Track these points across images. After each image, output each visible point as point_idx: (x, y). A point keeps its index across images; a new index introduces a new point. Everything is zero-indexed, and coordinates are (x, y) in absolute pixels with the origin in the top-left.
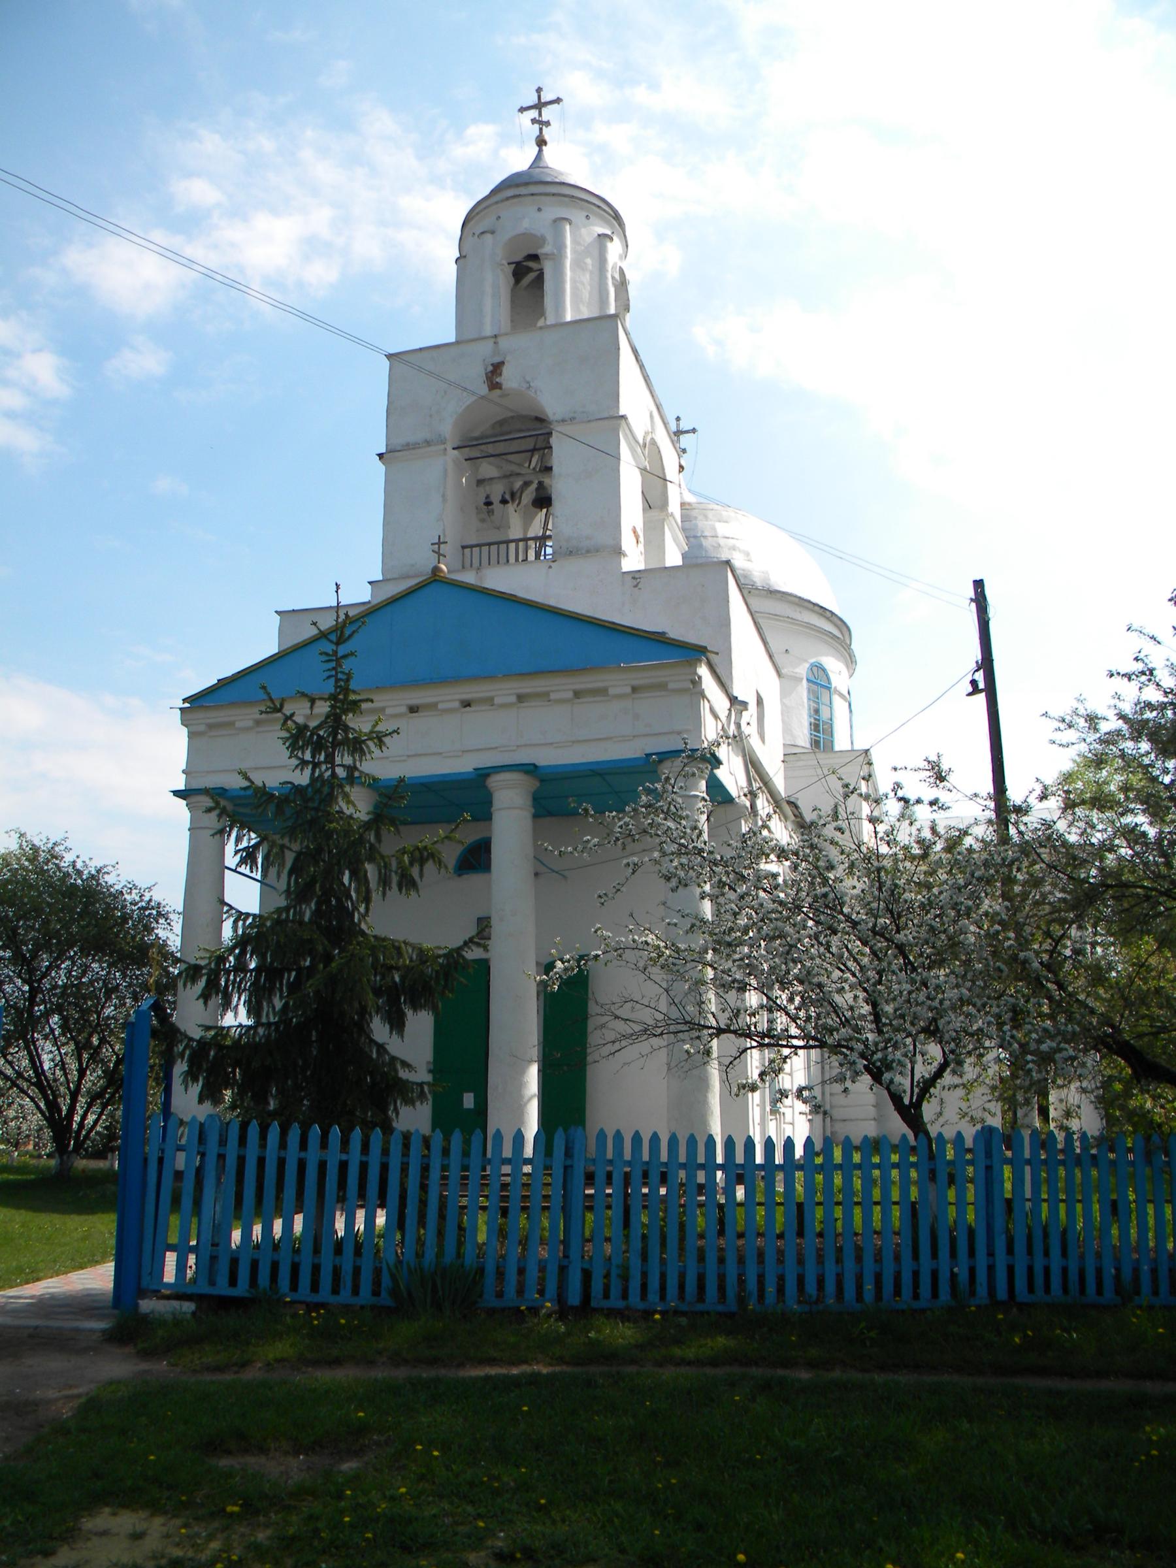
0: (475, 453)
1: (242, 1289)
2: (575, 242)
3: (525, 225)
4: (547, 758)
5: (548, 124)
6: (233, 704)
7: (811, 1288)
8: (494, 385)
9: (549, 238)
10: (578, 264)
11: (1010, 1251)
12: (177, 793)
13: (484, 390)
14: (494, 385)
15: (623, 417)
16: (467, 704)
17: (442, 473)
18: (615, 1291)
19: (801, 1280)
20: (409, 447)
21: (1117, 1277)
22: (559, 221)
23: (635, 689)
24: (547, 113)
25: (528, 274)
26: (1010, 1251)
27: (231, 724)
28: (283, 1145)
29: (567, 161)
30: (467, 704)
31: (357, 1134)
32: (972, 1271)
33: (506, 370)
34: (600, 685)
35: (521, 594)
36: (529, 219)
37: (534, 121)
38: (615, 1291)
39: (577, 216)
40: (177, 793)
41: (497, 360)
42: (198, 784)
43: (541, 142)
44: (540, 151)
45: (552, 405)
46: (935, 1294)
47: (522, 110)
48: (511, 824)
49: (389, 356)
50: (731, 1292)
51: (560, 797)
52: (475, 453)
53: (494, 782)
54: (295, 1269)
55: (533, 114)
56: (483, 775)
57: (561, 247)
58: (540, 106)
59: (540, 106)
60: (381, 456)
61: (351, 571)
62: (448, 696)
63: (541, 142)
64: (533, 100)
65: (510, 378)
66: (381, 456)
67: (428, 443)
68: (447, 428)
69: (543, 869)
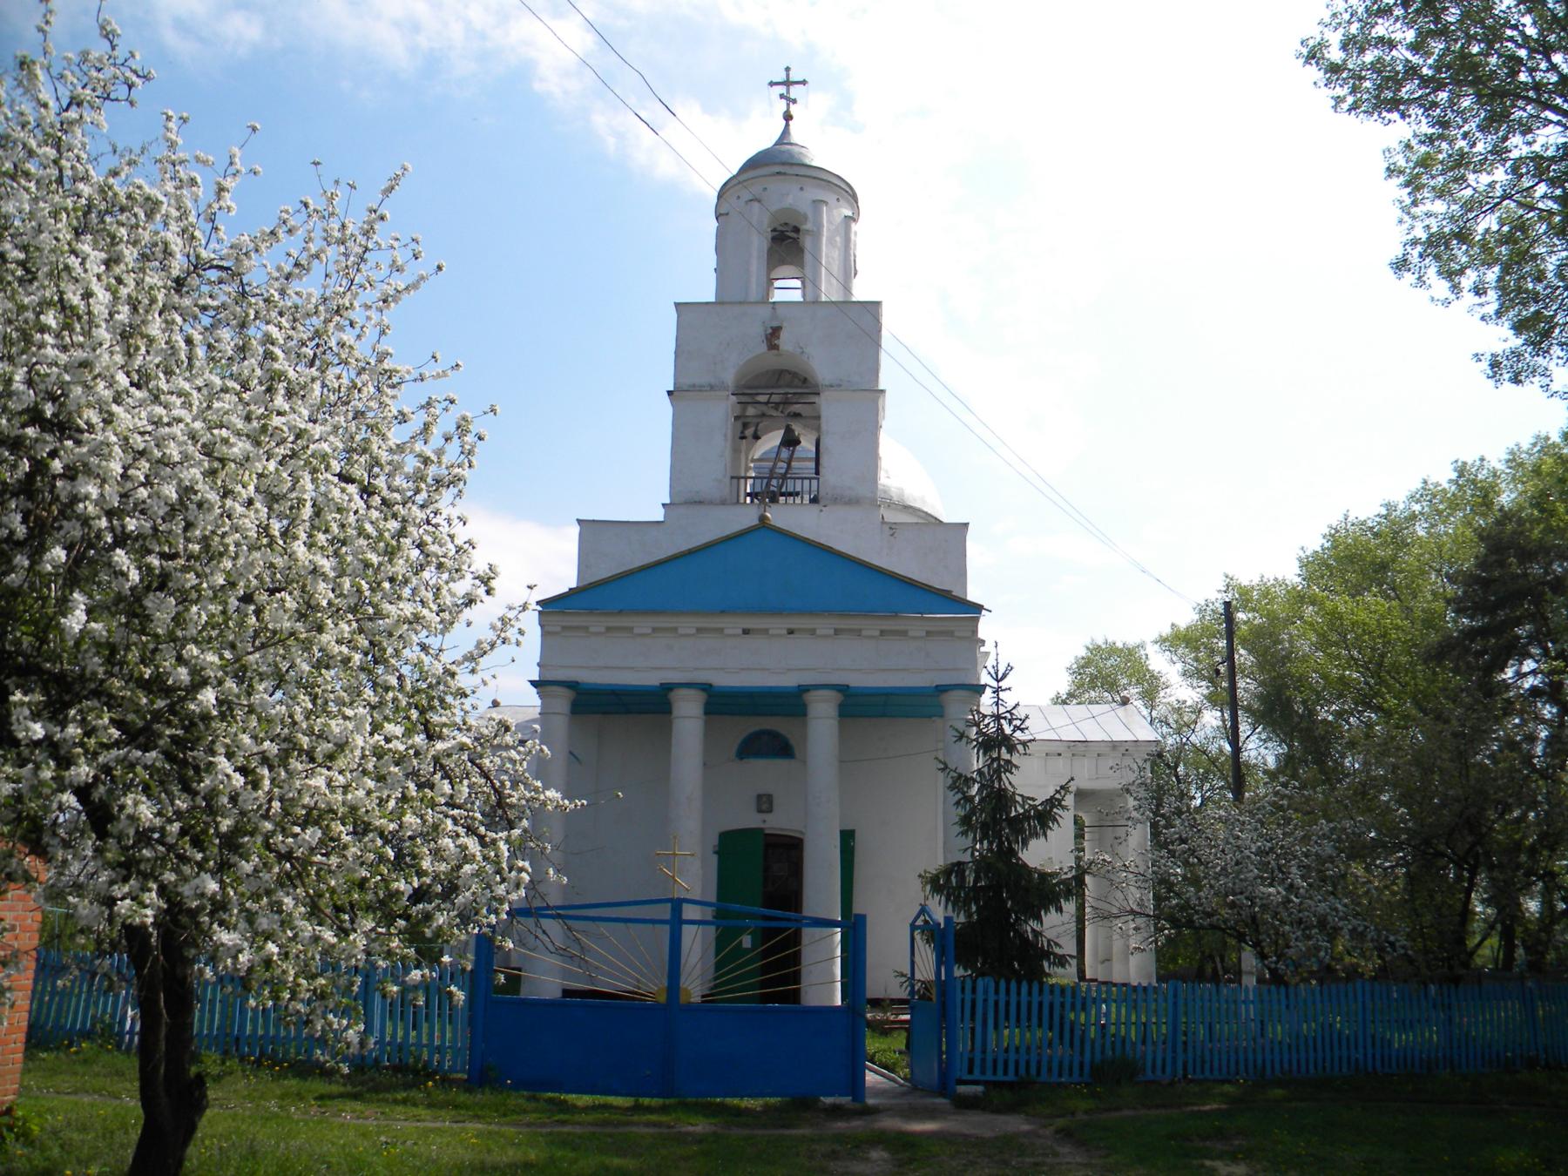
0: (744, 399)
1: (1011, 1077)
2: (829, 222)
3: (789, 201)
4: (856, 681)
5: (794, 101)
6: (591, 611)
7: (1286, 1066)
8: (773, 347)
9: (810, 215)
10: (831, 241)
11: (1374, 1045)
12: (533, 683)
13: (764, 348)
14: (773, 347)
15: (883, 391)
16: (791, 632)
17: (720, 412)
18: (1198, 1070)
19: (1281, 1061)
20: (695, 388)
21: (1092, 1062)
22: (818, 203)
23: (928, 633)
24: (795, 92)
25: (788, 243)
26: (1374, 1045)
27: (586, 628)
28: (1030, 993)
29: (819, 146)
30: (791, 632)
31: (1013, 985)
32: (1365, 1055)
33: (784, 335)
34: (902, 628)
35: (798, 532)
36: (794, 197)
37: (782, 96)
38: (1198, 1070)
39: (831, 197)
40: (533, 683)
41: (775, 324)
42: (549, 677)
43: (788, 117)
44: (787, 125)
45: (822, 369)
46: (1163, 1071)
47: (772, 84)
48: (822, 728)
49: (677, 305)
50: (1224, 1069)
51: (860, 706)
52: (744, 399)
53: (811, 697)
54: (995, 1062)
55: (782, 90)
56: (803, 690)
57: (819, 226)
58: (788, 83)
59: (788, 83)
60: (670, 393)
61: (640, 491)
62: (778, 625)
63: (788, 117)
64: (782, 77)
65: (786, 342)
66: (670, 393)
67: (712, 388)
68: (729, 377)
69: (847, 760)
